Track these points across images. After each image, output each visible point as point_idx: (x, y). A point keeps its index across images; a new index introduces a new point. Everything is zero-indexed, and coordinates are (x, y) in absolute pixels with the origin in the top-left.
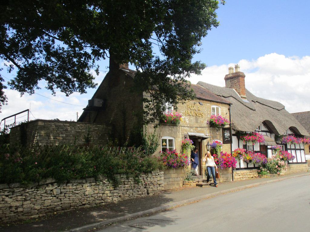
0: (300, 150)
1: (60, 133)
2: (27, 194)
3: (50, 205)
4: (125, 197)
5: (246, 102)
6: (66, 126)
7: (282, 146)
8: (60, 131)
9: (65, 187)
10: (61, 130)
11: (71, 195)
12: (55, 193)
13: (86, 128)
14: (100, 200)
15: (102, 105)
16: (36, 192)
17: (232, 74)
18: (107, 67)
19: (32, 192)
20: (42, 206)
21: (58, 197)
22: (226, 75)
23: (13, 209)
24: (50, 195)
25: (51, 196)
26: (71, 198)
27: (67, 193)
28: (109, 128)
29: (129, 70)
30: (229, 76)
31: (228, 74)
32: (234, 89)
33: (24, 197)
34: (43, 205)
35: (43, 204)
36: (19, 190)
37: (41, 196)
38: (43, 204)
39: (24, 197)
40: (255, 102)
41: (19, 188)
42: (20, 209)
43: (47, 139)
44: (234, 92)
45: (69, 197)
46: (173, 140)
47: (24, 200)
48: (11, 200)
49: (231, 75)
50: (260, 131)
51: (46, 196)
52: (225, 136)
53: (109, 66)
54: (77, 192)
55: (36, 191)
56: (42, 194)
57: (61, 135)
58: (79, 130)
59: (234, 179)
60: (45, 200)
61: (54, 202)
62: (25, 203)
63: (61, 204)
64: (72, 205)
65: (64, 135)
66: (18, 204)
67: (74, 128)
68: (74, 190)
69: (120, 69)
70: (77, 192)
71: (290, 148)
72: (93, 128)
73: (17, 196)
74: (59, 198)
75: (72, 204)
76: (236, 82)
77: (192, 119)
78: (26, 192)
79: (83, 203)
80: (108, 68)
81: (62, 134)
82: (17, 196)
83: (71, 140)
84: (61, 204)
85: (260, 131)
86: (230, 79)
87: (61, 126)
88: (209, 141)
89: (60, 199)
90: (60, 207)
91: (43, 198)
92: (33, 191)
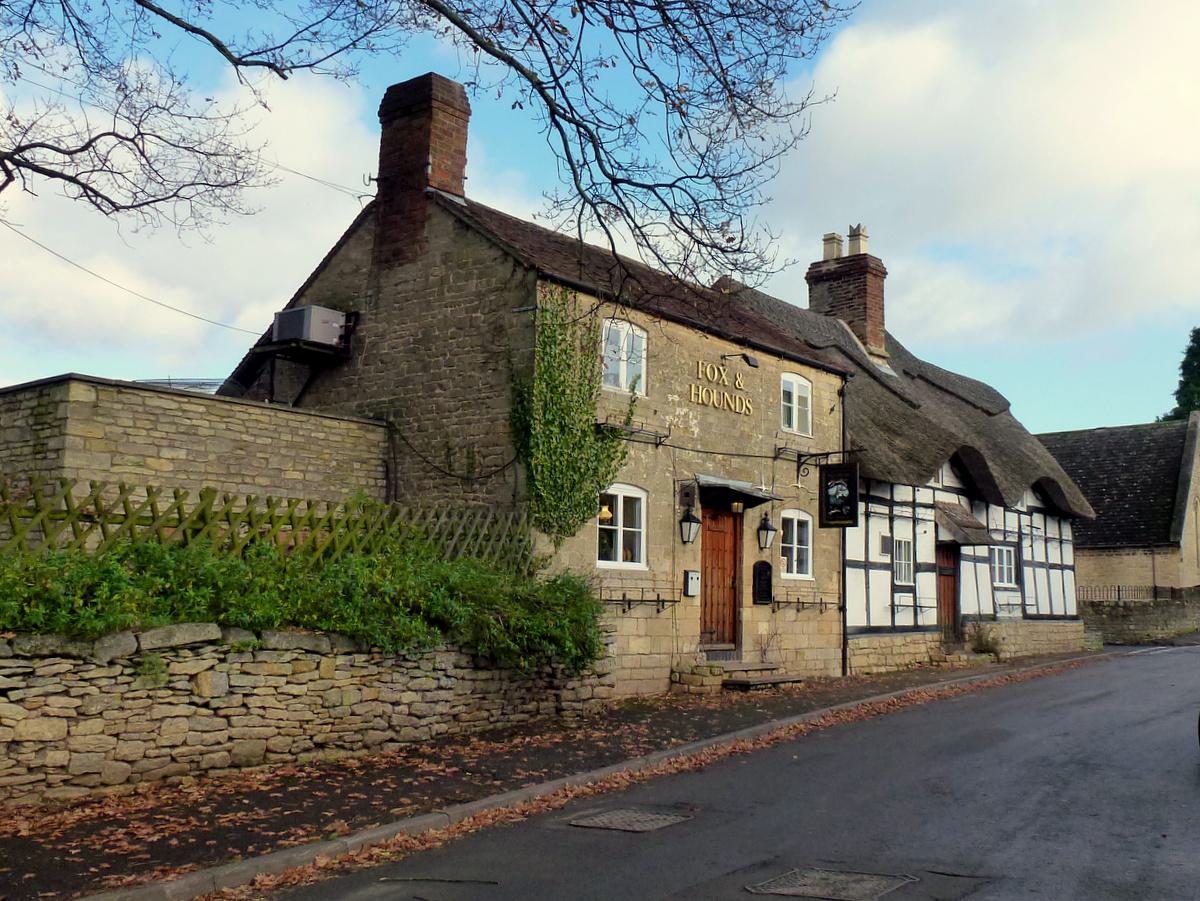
0: (1062, 567)
1: (165, 443)
2: (94, 690)
3: (185, 743)
4: (476, 723)
5: (888, 376)
6: (190, 415)
7: (1008, 551)
8: (164, 435)
9: (248, 668)
10: (167, 428)
11: (270, 701)
12: (207, 692)
13: (275, 431)
14: (384, 730)
15: (341, 337)
16: (128, 683)
17: (839, 260)
18: (370, 179)
19: (113, 681)
20: (152, 745)
21: (216, 710)
22: (815, 265)
23: (28, 754)
24: (187, 700)
25: (192, 703)
26: (269, 713)
27: (255, 691)
28: (370, 436)
29: (466, 201)
30: (824, 269)
31: (821, 259)
32: (841, 322)
33: (78, 702)
34: (154, 740)
35: (154, 735)
36: (55, 669)
37: (150, 701)
38: (154, 735)
39: (78, 702)
40: (913, 378)
41: (57, 660)
42: (58, 757)
43: (107, 466)
44: (844, 332)
45: (261, 712)
46: (639, 499)
47: (73, 713)
48: (18, 713)
49: (833, 266)
50: (938, 489)
51: (170, 704)
52: (849, 488)
53: (375, 175)
54: (295, 690)
55: (130, 675)
56: (151, 693)
57: (166, 453)
58: (245, 437)
59: (848, 670)
60: (162, 720)
61: (203, 732)
62: (84, 726)
63: (230, 739)
64: (271, 747)
65: (182, 454)
66: (49, 730)
67: (224, 426)
68: (284, 679)
69: (429, 189)
70: (295, 690)
71: (889, 624)
72: (306, 433)
73: (47, 695)
74: (222, 712)
75: (272, 743)
76: (850, 295)
77: (711, 419)
78: (82, 680)
79: (318, 739)
80: (375, 183)
81: (171, 446)
82: (47, 695)
83: (210, 477)
84: (230, 739)
85: (938, 489)
86: (828, 280)
87: (168, 412)
88: (770, 513)
89: (226, 717)
90: (226, 753)
91: (159, 711)
92: (115, 677)
